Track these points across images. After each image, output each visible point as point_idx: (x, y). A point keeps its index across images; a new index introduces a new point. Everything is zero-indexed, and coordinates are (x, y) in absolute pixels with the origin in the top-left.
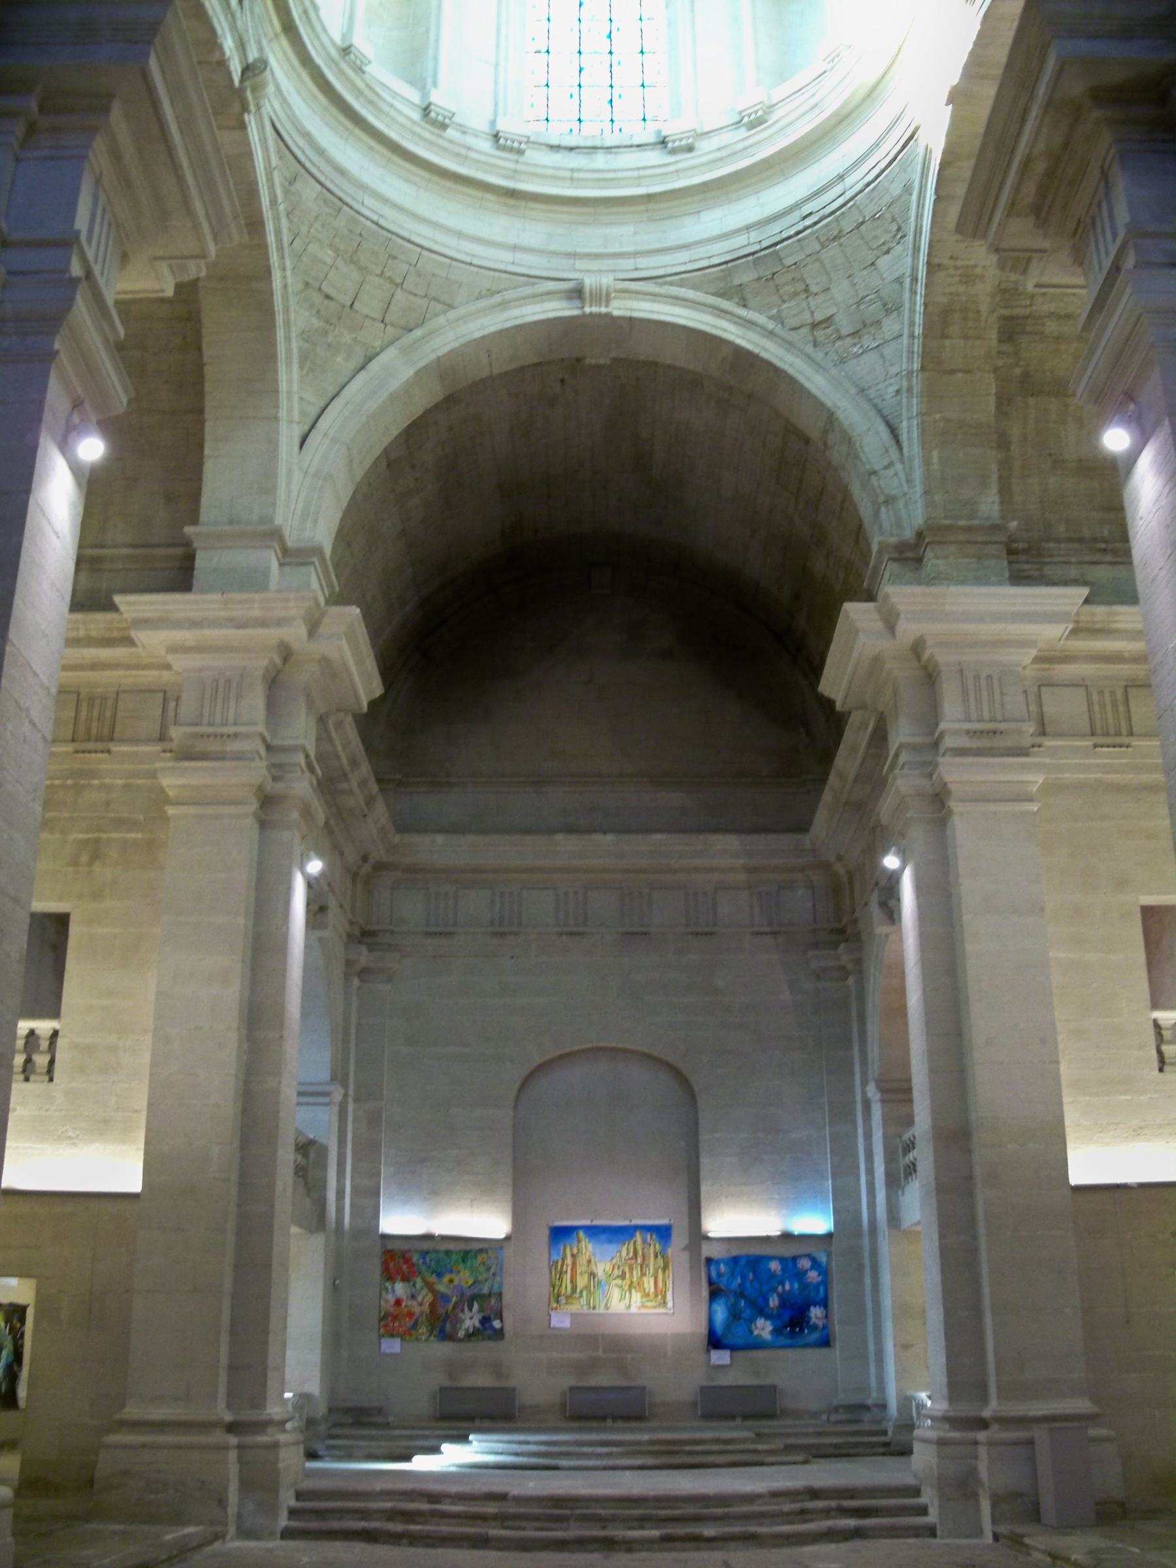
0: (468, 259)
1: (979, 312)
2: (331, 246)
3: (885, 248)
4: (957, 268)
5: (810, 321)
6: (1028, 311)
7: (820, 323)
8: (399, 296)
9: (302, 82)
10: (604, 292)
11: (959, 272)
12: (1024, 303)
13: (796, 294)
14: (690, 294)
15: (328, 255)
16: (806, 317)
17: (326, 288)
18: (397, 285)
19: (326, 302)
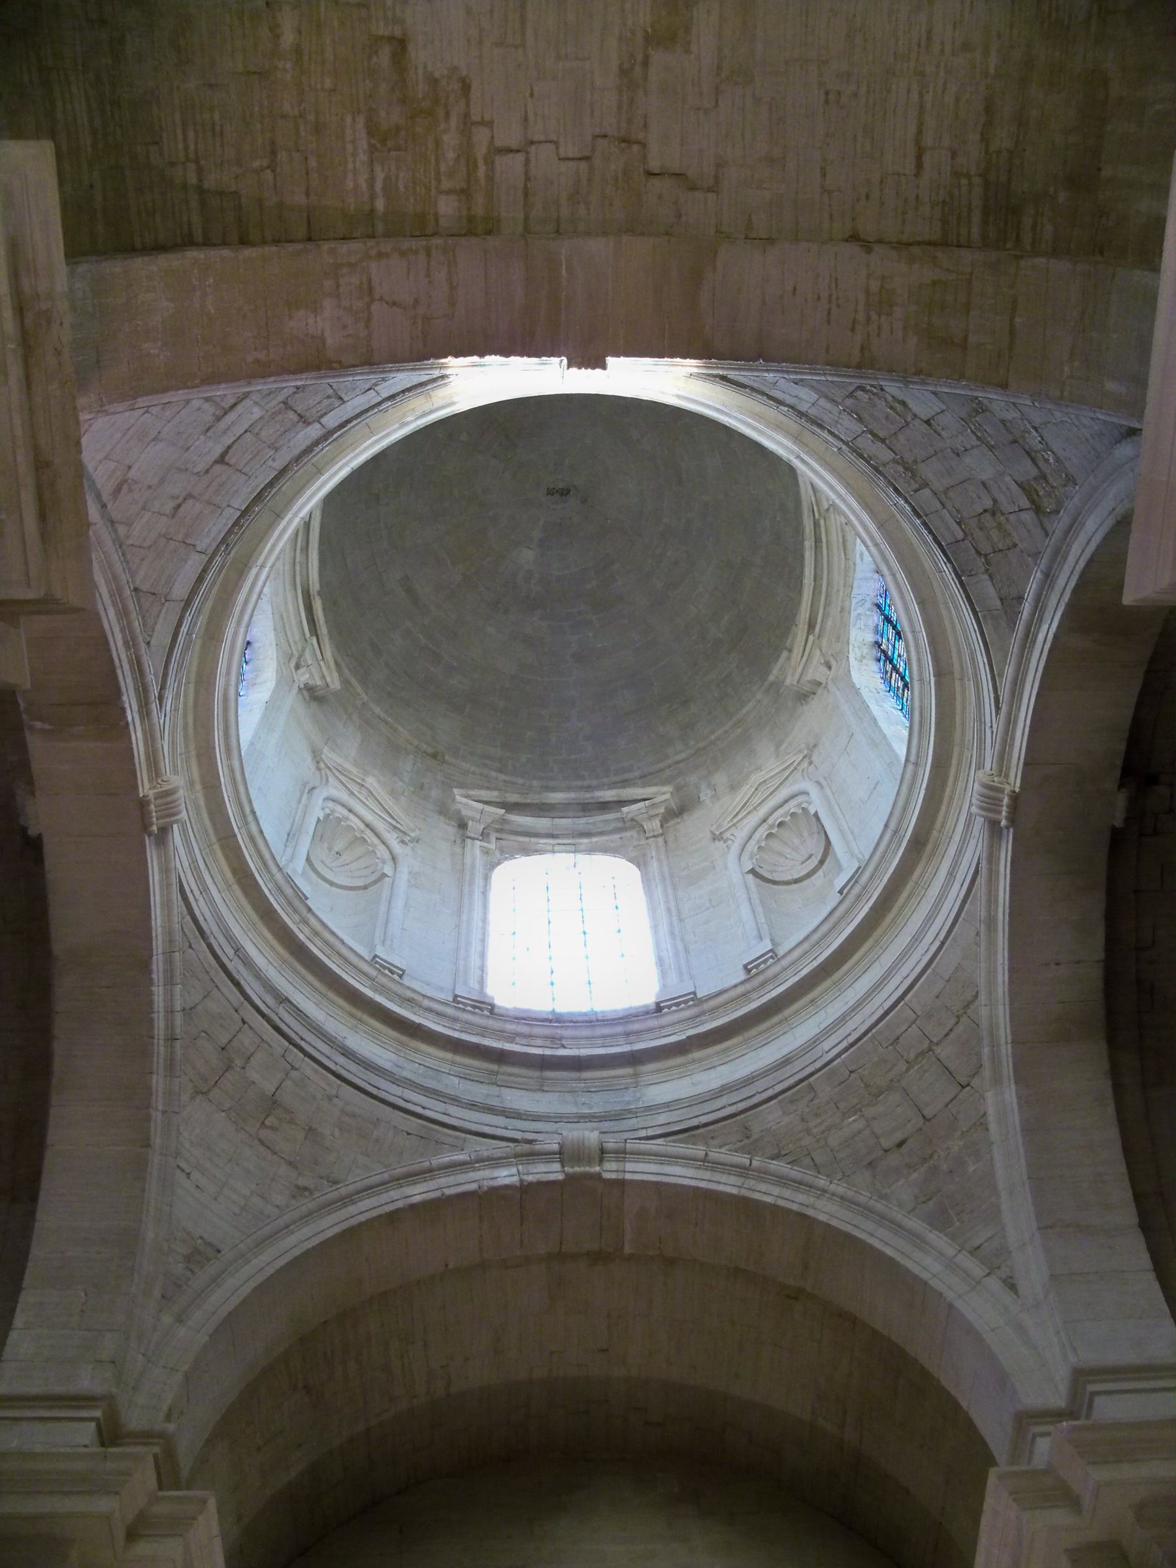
0: (937, 944)
1: (934, 283)
2: (845, 1115)
3: (899, 407)
4: (868, 320)
5: (1031, 513)
6: (977, 180)
7: (1033, 502)
8: (945, 1051)
9: (700, 1060)
10: (987, 792)
11: (874, 316)
12: (964, 189)
13: (1000, 526)
14: (1009, 671)
15: (854, 1123)
16: (1028, 517)
17: (886, 1143)
18: (930, 1049)
19: (904, 1149)
